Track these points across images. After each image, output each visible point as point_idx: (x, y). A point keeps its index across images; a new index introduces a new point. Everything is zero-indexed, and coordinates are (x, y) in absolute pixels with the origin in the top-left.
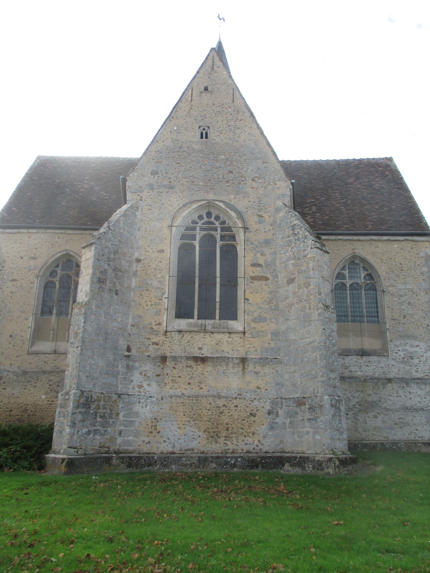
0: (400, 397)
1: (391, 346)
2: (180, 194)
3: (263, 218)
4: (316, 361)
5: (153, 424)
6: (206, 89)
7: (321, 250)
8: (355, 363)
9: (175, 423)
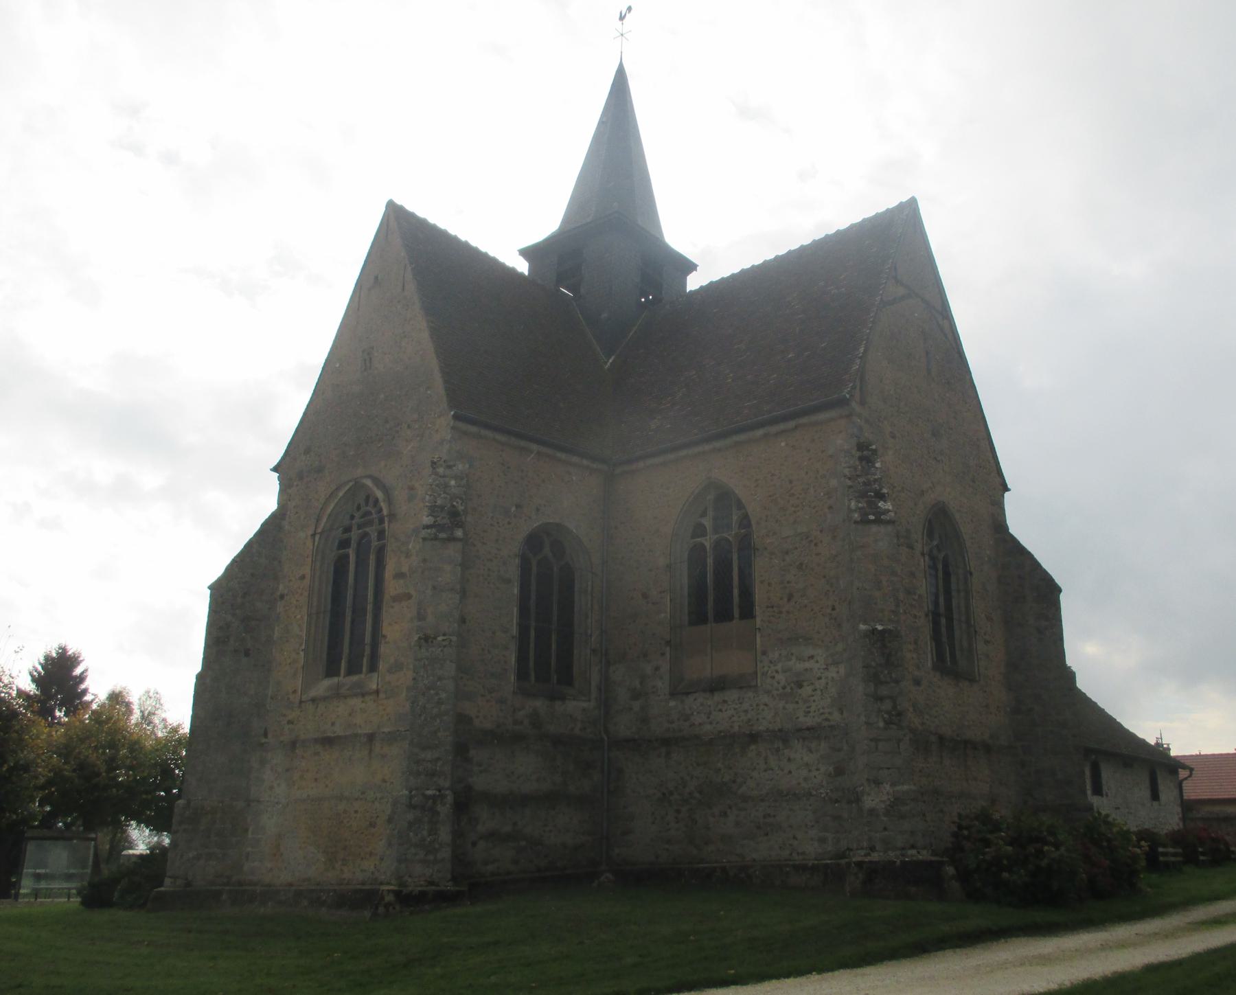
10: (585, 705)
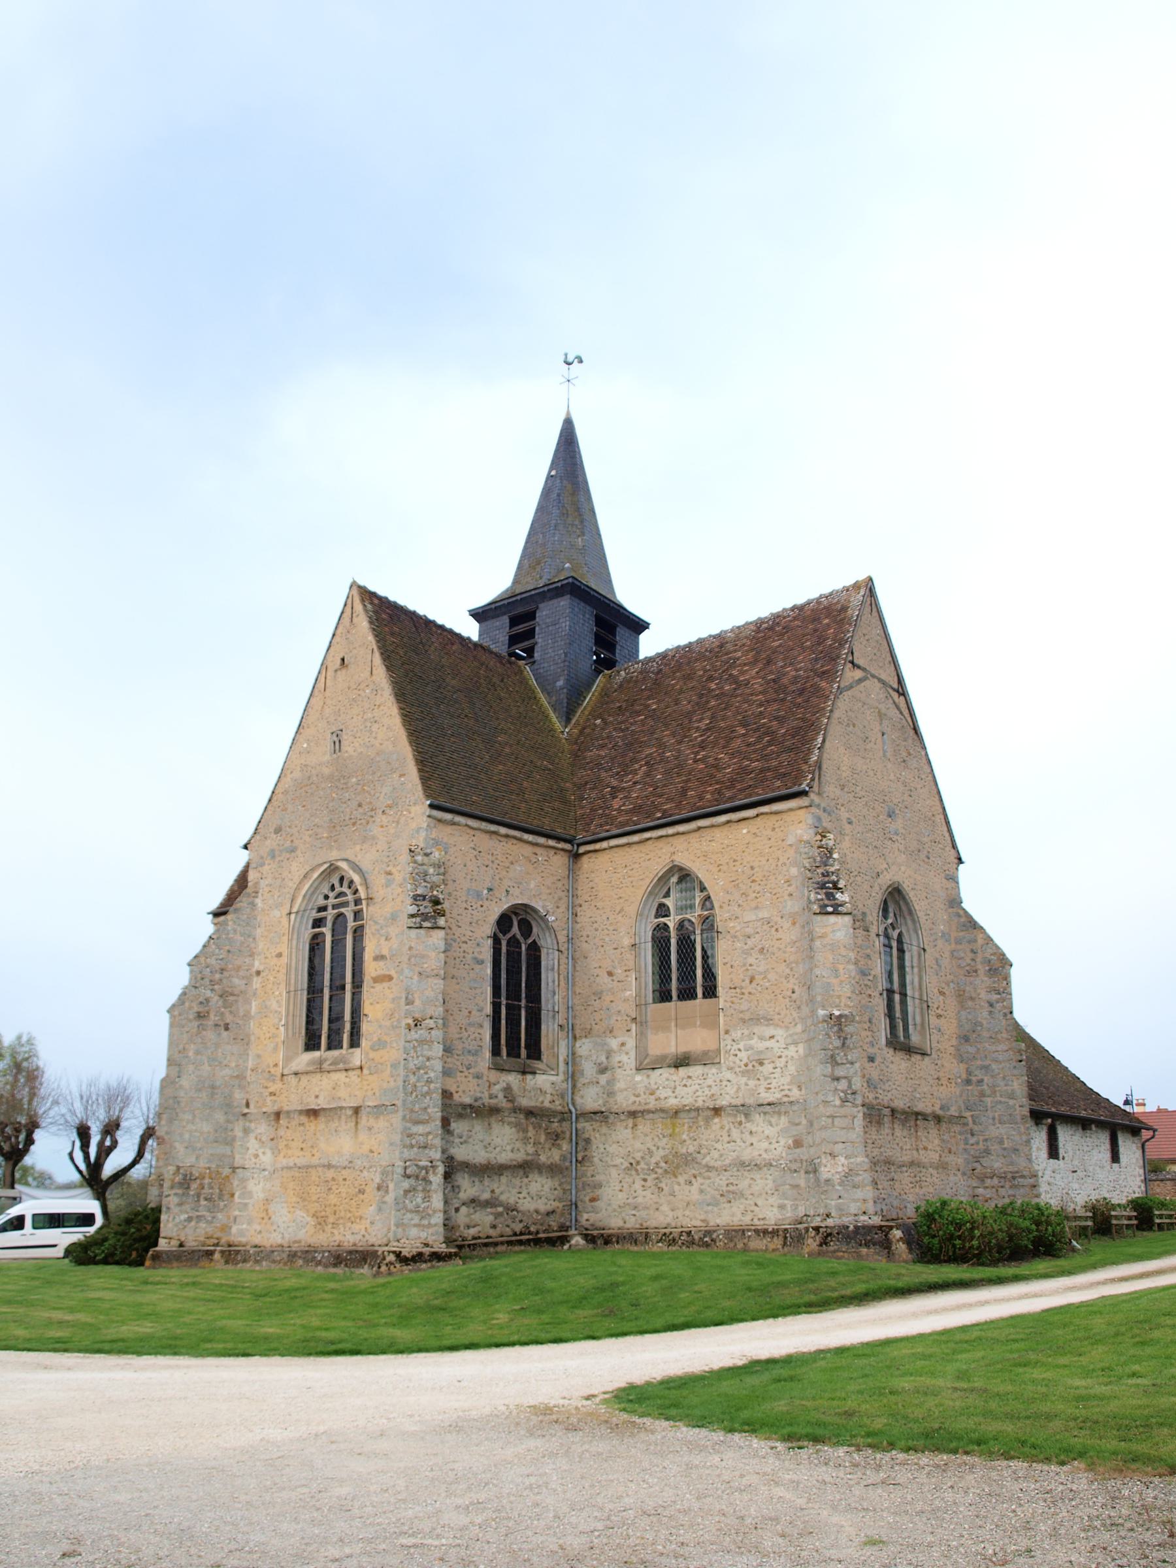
10: (554, 1078)
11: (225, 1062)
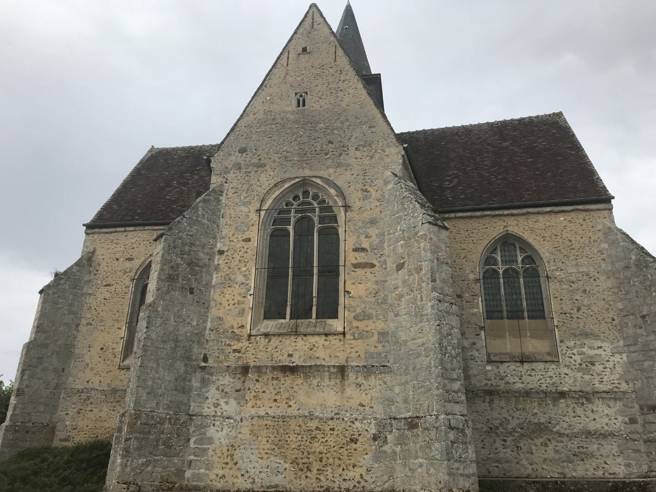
0: (579, 418)
1: (562, 348)
2: (271, 173)
3: (369, 193)
4: (431, 368)
5: (230, 453)
6: (304, 50)
7: (436, 225)
8: (514, 372)
9: (256, 451)
11: (188, 320)
